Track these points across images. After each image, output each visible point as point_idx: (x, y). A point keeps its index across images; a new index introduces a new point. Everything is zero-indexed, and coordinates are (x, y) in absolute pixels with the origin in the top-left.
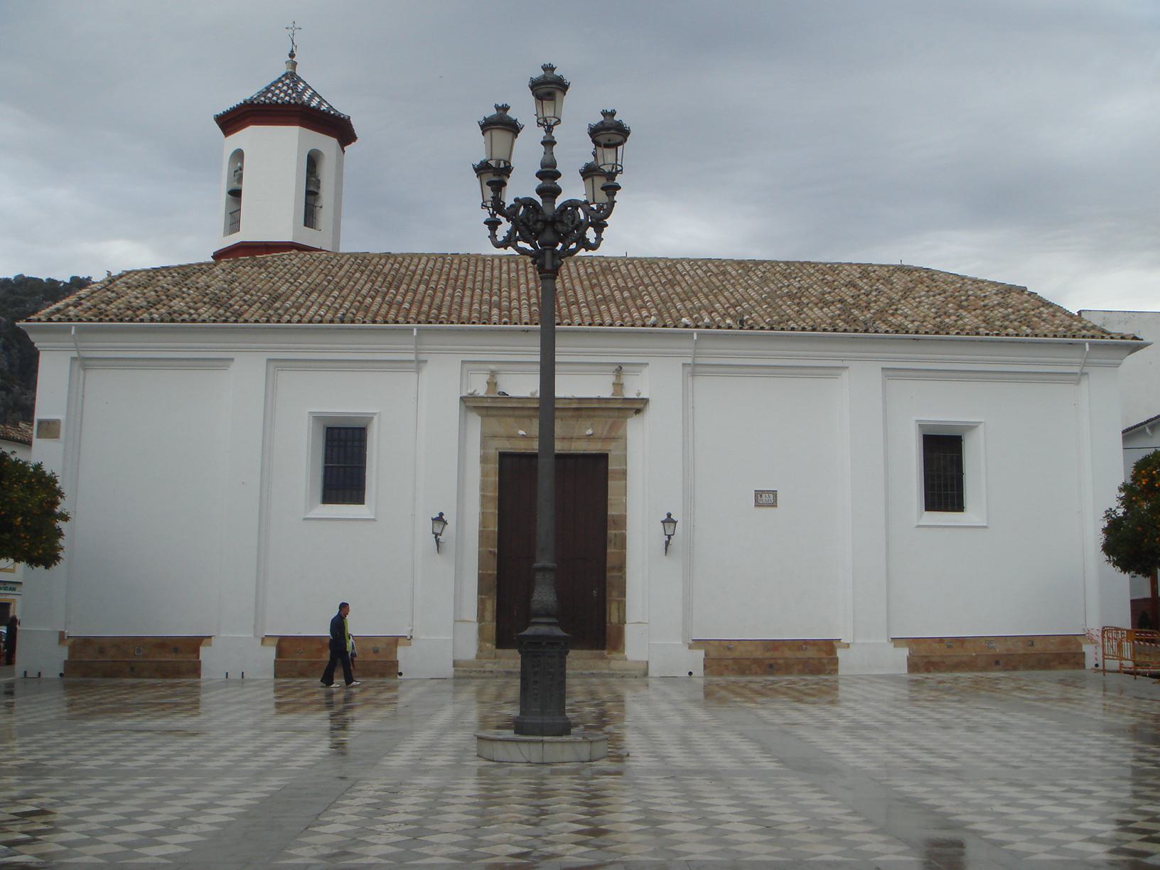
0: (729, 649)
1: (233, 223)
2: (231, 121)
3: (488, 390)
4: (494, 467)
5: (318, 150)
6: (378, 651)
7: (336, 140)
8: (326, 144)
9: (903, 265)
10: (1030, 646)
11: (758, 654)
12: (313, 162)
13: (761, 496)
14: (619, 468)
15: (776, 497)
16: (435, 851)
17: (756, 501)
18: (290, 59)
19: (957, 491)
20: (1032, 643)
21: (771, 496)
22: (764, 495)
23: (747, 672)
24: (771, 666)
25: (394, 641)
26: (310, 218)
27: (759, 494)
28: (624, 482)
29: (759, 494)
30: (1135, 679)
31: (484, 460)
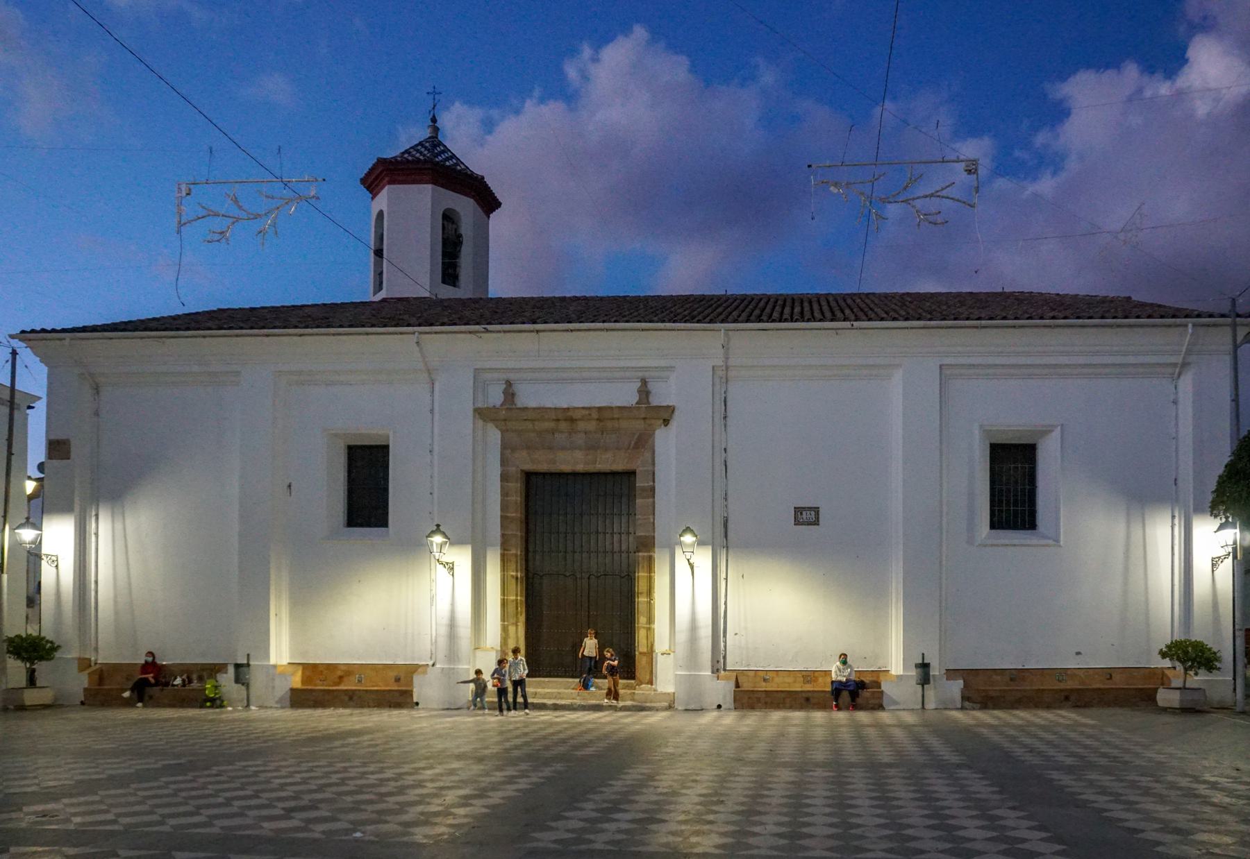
0: (765, 680)
1: (379, 286)
2: (374, 180)
3: (505, 400)
4: (516, 486)
5: (454, 210)
6: (399, 679)
7: (472, 200)
8: (465, 206)
9: (1005, 292)
10: (1108, 679)
11: (797, 687)
12: (449, 217)
13: (801, 514)
14: (646, 485)
15: (818, 515)
16: (785, 719)
17: (810, 524)
18: (431, 124)
19: (1025, 489)
20: (1111, 676)
21: (813, 513)
22: (804, 513)
23: (781, 705)
24: (808, 699)
25: (413, 669)
26: (450, 275)
27: (799, 511)
28: (651, 500)
29: (799, 511)
30: (837, 334)
31: (504, 478)
